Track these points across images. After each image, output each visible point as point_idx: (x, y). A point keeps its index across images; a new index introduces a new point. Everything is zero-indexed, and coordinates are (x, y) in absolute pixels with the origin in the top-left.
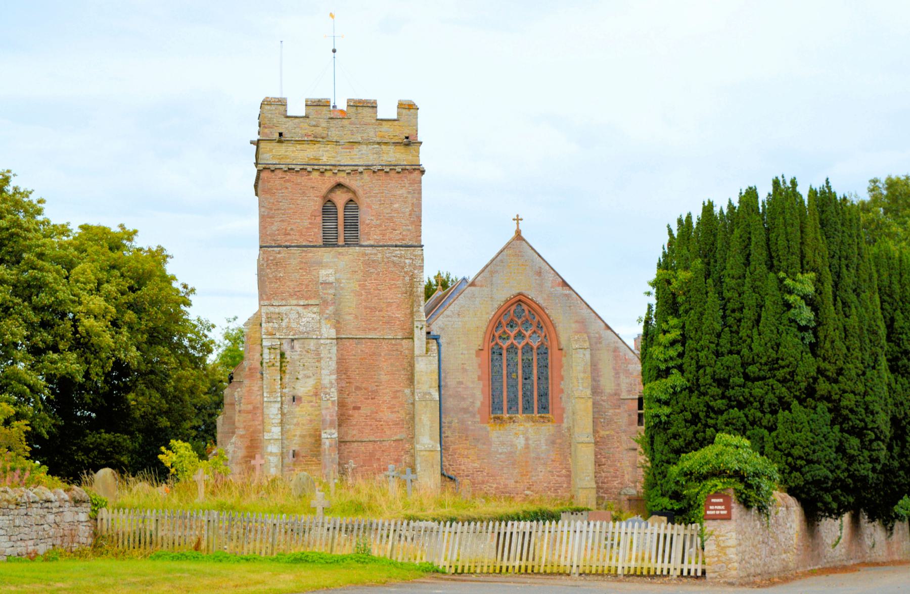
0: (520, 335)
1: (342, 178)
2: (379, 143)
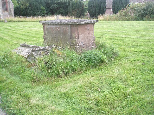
2: (78, 31)
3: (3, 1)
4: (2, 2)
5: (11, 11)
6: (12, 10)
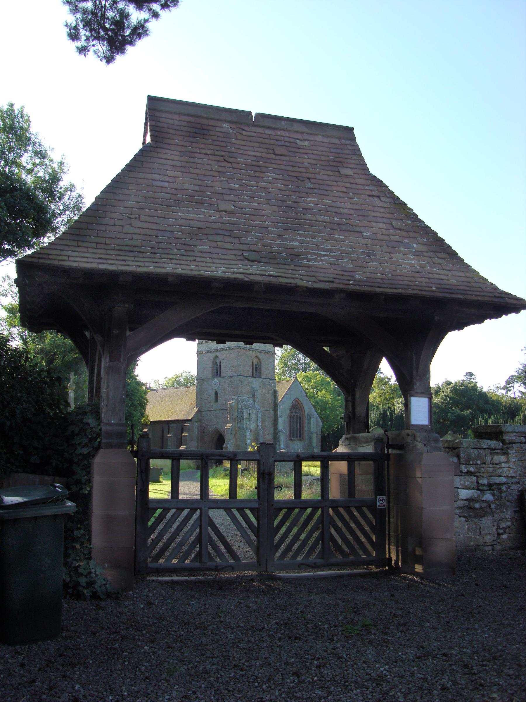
0: (295, 412)
1: (258, 354)
3: (292, 415)
4: (290, 416)
5: (310, 439)
6: (314, 436)
